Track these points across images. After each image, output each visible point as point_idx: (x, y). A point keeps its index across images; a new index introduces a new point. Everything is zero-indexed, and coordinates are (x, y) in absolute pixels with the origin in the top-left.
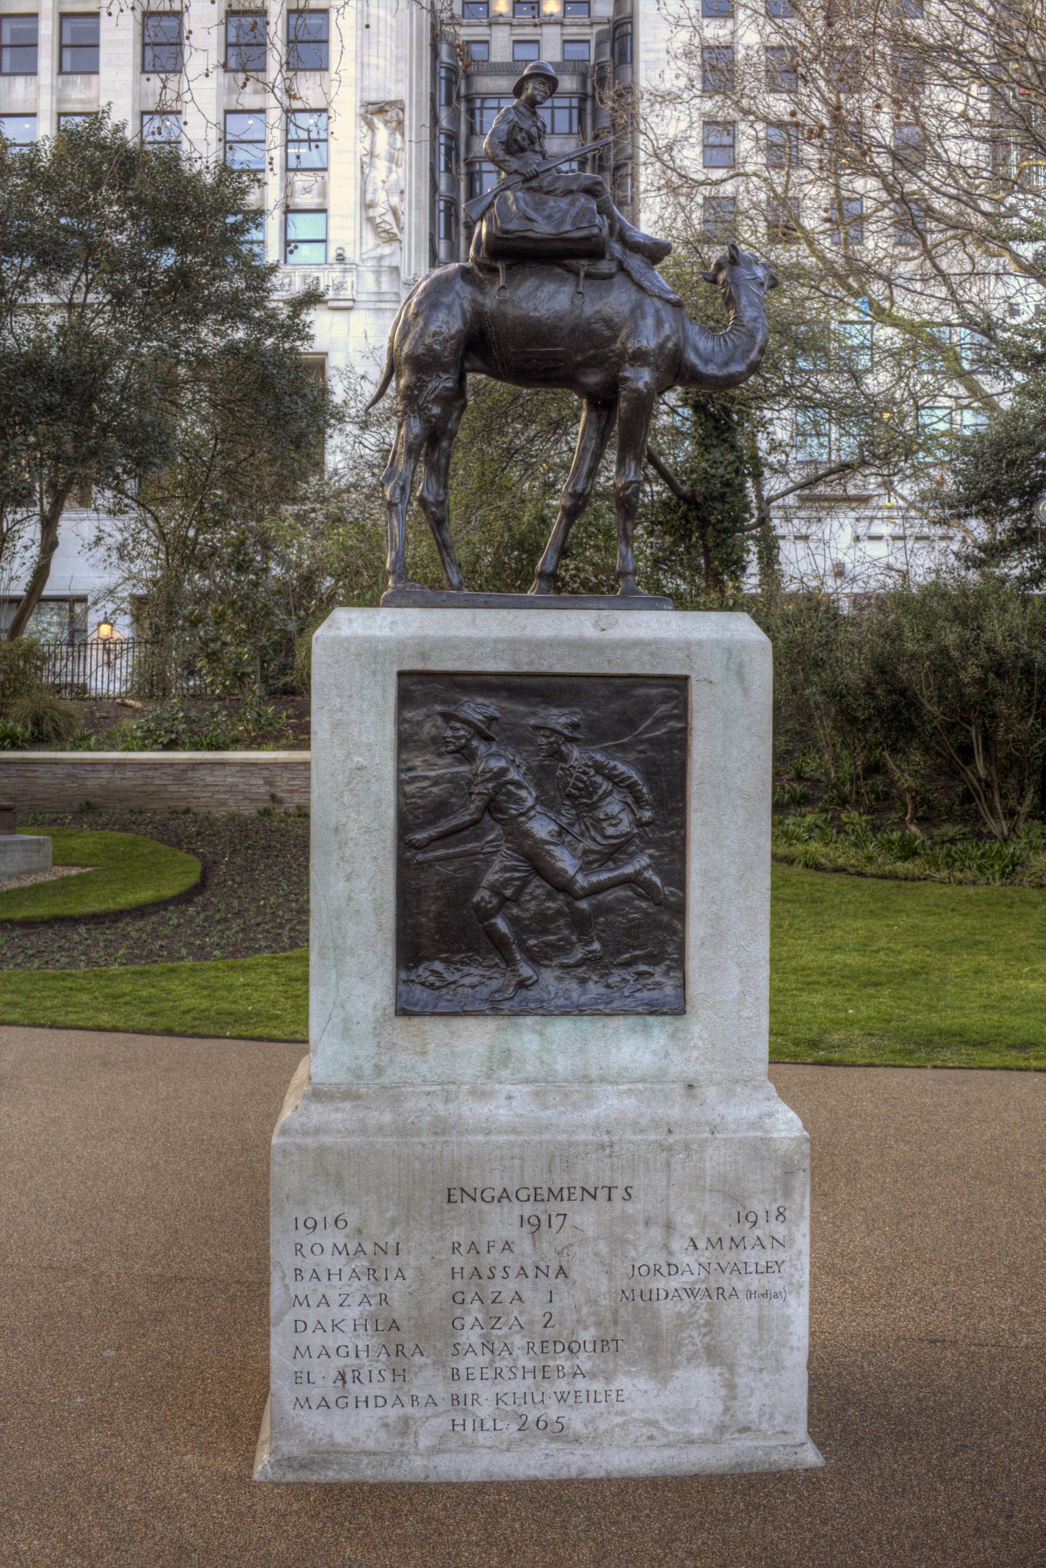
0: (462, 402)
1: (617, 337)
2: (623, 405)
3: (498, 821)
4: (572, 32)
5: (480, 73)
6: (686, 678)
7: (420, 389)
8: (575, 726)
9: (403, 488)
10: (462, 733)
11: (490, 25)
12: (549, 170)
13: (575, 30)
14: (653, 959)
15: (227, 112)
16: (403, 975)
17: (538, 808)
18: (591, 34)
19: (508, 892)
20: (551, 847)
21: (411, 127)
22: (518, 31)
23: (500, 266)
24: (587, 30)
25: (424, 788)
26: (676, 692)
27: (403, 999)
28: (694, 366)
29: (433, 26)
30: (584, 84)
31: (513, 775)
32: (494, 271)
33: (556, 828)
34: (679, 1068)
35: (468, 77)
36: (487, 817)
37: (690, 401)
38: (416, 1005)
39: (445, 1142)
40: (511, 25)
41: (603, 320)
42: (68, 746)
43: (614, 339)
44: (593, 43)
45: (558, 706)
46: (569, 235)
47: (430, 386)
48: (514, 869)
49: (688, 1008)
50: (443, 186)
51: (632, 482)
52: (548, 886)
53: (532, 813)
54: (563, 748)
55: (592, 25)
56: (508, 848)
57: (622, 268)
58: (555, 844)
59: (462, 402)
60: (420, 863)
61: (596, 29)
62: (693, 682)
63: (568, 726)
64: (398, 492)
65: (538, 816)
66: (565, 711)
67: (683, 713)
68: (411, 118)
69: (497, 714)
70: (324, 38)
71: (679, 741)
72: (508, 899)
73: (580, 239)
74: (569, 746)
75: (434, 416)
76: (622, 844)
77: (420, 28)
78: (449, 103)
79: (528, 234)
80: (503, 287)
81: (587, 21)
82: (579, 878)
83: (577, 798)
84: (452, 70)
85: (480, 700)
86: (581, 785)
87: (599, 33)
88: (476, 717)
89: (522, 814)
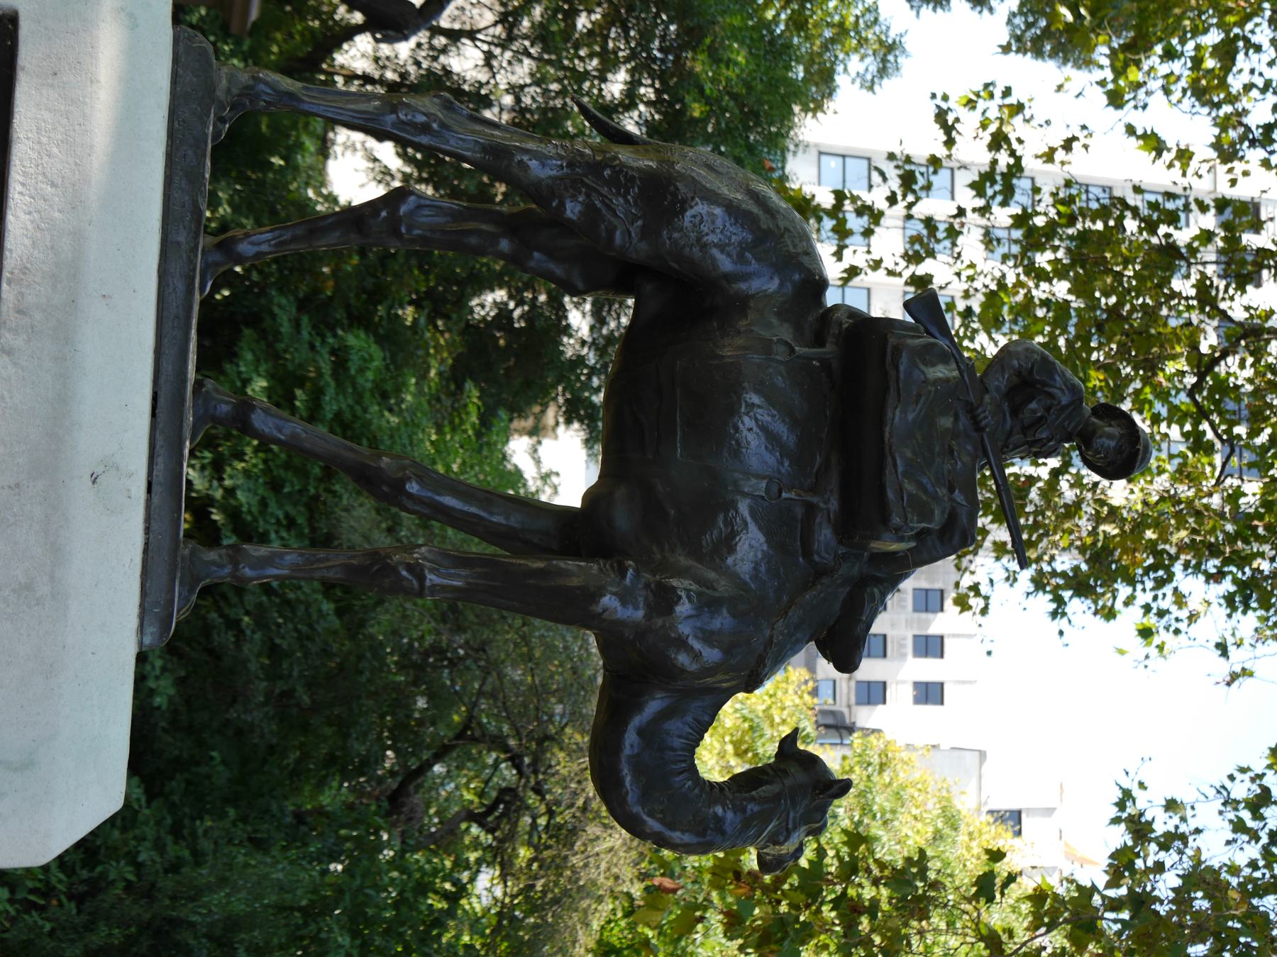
0: (580, 285)
1: (700, 560)
7: (613, 182)
9: (425, 129)
12: (986, 455)
15: (869, 290)
23: (829, 348)
24: (844, 702)
28: (639, 708)
32: (819, 341)
34: (948, 885)
41: (733, 535)
43: (696, 552)
46: (888, 470)
47: (618, 202)
51: (421, 578)
55: (849, 706)
57: (820, 572)
59: (580, 285)
61: (845, 710)
64: (421, 119)
73: (882, 489)
75: (562, 205)
79: (893, 393)
80: (792, 350)
87: (842, 714)
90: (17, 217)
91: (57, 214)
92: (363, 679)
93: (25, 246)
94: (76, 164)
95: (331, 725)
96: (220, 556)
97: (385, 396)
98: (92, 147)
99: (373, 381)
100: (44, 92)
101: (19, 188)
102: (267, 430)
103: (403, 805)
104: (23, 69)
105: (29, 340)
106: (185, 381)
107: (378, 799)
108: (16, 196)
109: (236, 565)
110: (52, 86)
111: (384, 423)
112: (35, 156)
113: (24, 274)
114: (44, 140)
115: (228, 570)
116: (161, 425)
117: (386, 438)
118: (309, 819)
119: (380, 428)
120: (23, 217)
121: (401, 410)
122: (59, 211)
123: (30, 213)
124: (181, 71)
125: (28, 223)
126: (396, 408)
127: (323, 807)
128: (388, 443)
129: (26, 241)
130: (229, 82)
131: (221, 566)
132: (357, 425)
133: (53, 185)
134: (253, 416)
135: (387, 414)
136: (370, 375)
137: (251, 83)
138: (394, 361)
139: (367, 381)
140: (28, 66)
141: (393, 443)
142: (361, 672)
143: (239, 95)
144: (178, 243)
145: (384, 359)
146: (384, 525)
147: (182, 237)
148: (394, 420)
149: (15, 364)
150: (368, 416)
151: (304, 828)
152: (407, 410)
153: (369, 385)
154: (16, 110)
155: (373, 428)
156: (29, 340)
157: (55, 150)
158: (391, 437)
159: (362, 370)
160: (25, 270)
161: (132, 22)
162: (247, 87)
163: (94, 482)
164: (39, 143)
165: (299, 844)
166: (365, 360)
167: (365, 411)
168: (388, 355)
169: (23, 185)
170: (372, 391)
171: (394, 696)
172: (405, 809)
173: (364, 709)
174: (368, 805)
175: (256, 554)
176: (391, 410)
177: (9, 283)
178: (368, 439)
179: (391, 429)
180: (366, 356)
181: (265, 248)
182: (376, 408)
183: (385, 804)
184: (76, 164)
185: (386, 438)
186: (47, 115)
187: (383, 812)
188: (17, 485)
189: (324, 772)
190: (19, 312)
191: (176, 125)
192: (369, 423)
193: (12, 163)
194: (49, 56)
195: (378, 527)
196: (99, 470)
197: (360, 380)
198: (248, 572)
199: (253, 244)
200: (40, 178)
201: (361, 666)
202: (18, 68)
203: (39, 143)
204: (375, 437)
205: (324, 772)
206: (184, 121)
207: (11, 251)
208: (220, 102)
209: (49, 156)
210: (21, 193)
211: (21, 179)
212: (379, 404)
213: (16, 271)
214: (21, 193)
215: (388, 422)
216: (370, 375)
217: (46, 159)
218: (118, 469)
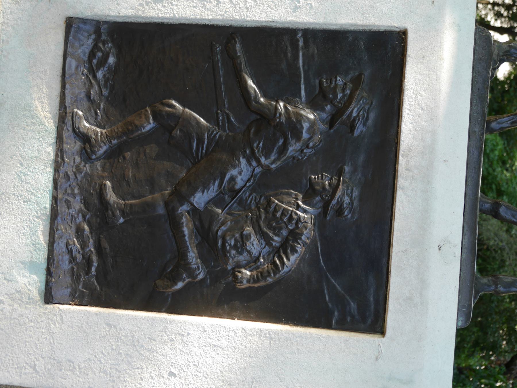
3: (248, 129)
8: (339, 211)
10: (340, 95)
14: (103, 275)
16: (104, 29)
17: (258, 170)
20: (217, 183)
26: (369, 321)
27: (82, 25)
31: (293, 148)
33: (237, 187)
36: (254, 117)
38: (74, 37)
39: (45, 117)
42: (455, 384)
45: (361, 199)
48: (200, 142)
53: (254, 164)
54: (318, 198)
56: (220, 137)
63: (340, 203)
65: (250, 169)
66: (356, 203)
67: (345, 324)
69: (356, 133)
72: (171, 133)
74: (320, 205)
82: (185, 207)
85: (372, 116)
86: (278, 214)
88: (354, 110)
89: (253, 152)
90: (406, 125)
91: (424, 123)
92: (493, 305)
93: (410, 138)
94: (433, 99)
95: (476, 326)
96: (489, 281)
97: (504, 163)
98: (440, 90)
99: (498, 156)
100: (419, 66)
101: (407, 112)
102: (507, 217)
103: (513, 370)
104: (409, 56)
105: (411, 183)
106: (477, 198)
107: (500, 365)
108: (406, 115)
109: (496, 285)
110: (422, 63)
111: (503, 177)
112: (414, 96)
113: (409, 152)
114: (419, 88)
115: (493, 288)
116: (466, 220)
117: (504, 184)
118: (465, 372)
119: (501, 179)
120: (408, 124)
121: (512, 170)
122: (425, 122)
123: (412, 123)
124: (477, 48)
125: (411, 128)
126: (510, 169)
127: (470, 366)
128: (506, 187)
129: (410, 136)
130: (498, 50)
131: (489, 286)
132: (490, 178)
133: (422, 109)
134: (500, 210)
135: (505, 172)
136: (497, 153)
137: (508, 49)
138: (508, 144)
139: (495, 156)
140: (411, 54)
141: (508, 187)
142: (493, 302)
143: (503, 56)
144: (475, 132)
145: (504, 144)
146: (505, 229)
147: (477, 129)
148: (508, 175)
149: (405, 194)
150: (496, 173)
151: (463, 376)
152: (515, 169)
153: (496, 158)
154: (406, 75)
155: (498, 179)
156: (411, 183)
157: (424, 93)
158: (507, 183)
159: (492, 150)
160: (410, 150)
161: (459, 29)
162: (506, 51)
163: (439, 249)
164: (416, 90)
165: (461, 385)
166: (494, 146)
167: (494, 170)
168: (506, 142)
169: (409, 110)
170: (497, 161)
171: (508, 314)
172: (514, 372)
173: (494, 320)
174: (495, 368)
175: (506, 280)
176: (507, 170)
177: (403, 157)
178: (495, 185)
179: (507, 180)
180: (495, 143)
181: (505, 125)
182: (499, 169)
183: (504, 369)
184: (433, 99)
185: (504, 184)
186: (420, 77)
187: (502, 373)
188: (406, 251)
189: (473, 349)
190: (407, 169)
191: (475, 74)
192: (495, 177)
193: (404, 100)
194: (421, 49)
195: (501, 229)
196: (442, 244)
197: (492, 155)
198: (501, 289)
199: (499, 123)
200: (417, 106)
201: (492, 298)
202: (407, 56)
203: (416, 90)
204: (499, 184)
205: (473, 349)
206: (478, 72)
207: (403, 141)
208: (495, 61)
209: (421, 96)
210: (408, 114)
211: (408, 107)
212: (501, 167)
213: (406, 151)
214: (408, 114)
215: (506, 176)
216: (497, 153)
217: (419, 97)
218: (450, 243)
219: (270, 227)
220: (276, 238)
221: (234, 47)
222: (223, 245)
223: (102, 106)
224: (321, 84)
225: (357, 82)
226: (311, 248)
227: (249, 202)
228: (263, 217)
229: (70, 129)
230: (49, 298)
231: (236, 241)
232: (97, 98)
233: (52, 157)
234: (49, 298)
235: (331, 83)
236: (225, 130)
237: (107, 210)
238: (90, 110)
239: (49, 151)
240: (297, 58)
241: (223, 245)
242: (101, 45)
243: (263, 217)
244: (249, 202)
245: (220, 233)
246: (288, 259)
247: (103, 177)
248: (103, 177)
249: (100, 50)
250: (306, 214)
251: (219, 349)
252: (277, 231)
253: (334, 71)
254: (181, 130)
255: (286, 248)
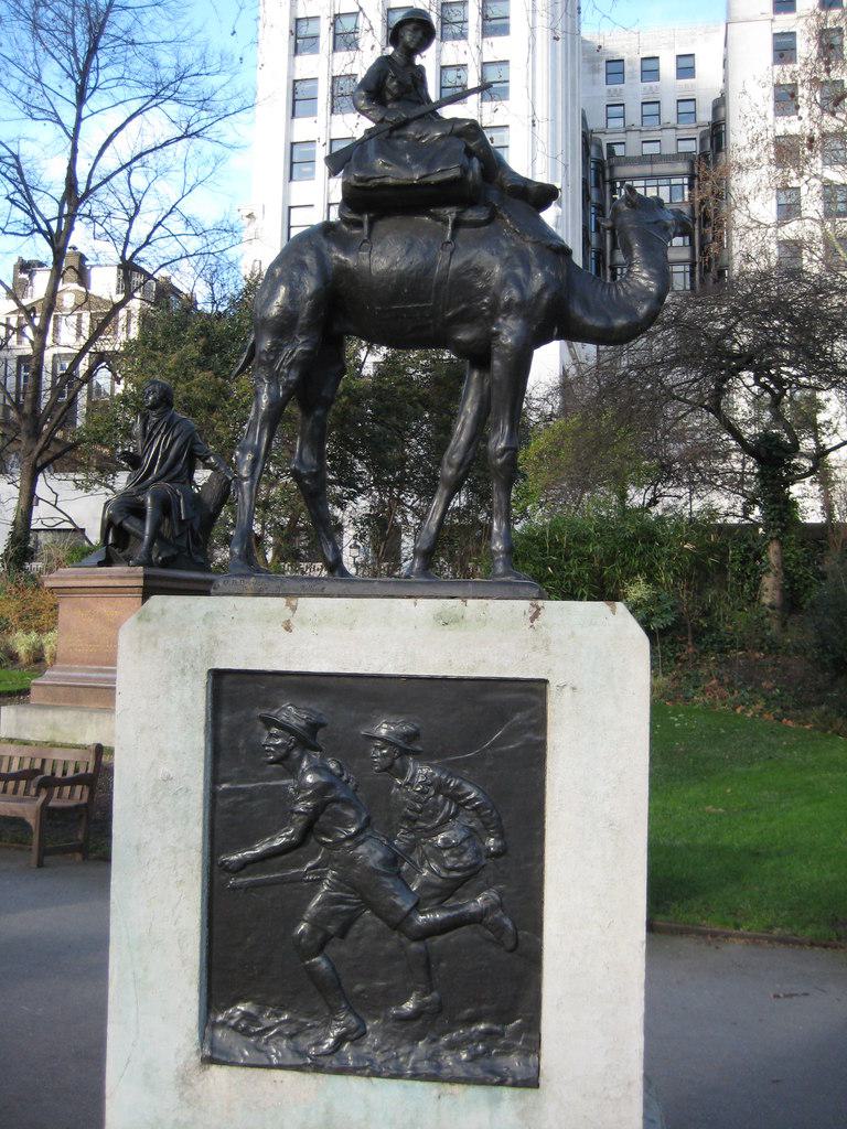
2: (496, 363)
4: (683, 134)
5: (619, 165)
6: (545, 682)
11: (626, 132)
13: (686, 132)
18: (696, 134)
19: (332, 928)
21: (567, 201)
22: (645, 134)
24: (694, 131)
25: (239, 803)
29: (584, 135)
30: (692, 168)
35: (611, 168)
37: (208, 323)
40: (640, 131)
44: (698, 140)
48: (340, 901)
49: (542, 1081)
50: (594, 242)
52: (381, 923)
58: (385, 874)
60: (234, 888)
62: (552, 689)
68: (567, 196)
70: (506, 144)
71: (534, 758)
76: (466, 879)
77: (573, 135)
78: (597, 185)
81: (694, 125)
83: (415, 821)
84: (599, 163)
219: (433, 816)
220: (447, 808)
221: (231, 862)
222: (458, 870)
223: (304, 1020)
224: (272, 762)
225: (269, 722)
226: (453, 769)
227: (614, 297)
228: (423, 824)
229: (330, 1059)
230: (532, 1082)
231: (452, 855)
232: (294, 1026)
233: (363, 1080)
234: (532, 1082)
235: (270, 751)
236: (327, 872)
237: (422, 1013)
238: (309, 1034)
239: (355, 1084)
240: (243, 791)
241: (458, 870)
242: (232, 1022)
243: (423, 824)
244: (614, 297)
245: (444, 874)
246: (469, 794)
247: (386, 1017)
248: (386, 1017)
249: (237, 1024)
250: (422, 772)
251: (22, 232)
252: (437, 808)
253: (257, 750)
254: (329, 924)
255: (455, 797)
